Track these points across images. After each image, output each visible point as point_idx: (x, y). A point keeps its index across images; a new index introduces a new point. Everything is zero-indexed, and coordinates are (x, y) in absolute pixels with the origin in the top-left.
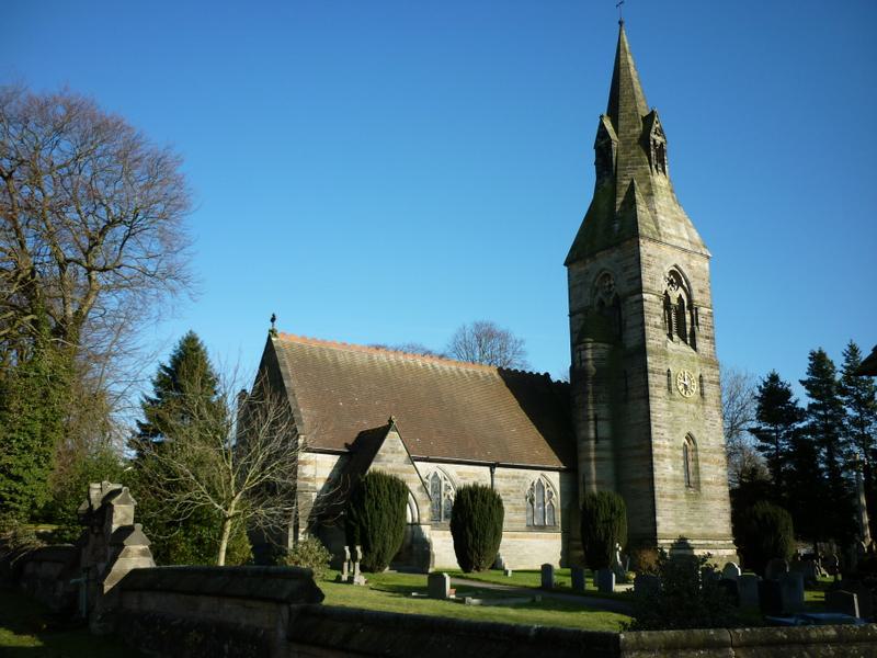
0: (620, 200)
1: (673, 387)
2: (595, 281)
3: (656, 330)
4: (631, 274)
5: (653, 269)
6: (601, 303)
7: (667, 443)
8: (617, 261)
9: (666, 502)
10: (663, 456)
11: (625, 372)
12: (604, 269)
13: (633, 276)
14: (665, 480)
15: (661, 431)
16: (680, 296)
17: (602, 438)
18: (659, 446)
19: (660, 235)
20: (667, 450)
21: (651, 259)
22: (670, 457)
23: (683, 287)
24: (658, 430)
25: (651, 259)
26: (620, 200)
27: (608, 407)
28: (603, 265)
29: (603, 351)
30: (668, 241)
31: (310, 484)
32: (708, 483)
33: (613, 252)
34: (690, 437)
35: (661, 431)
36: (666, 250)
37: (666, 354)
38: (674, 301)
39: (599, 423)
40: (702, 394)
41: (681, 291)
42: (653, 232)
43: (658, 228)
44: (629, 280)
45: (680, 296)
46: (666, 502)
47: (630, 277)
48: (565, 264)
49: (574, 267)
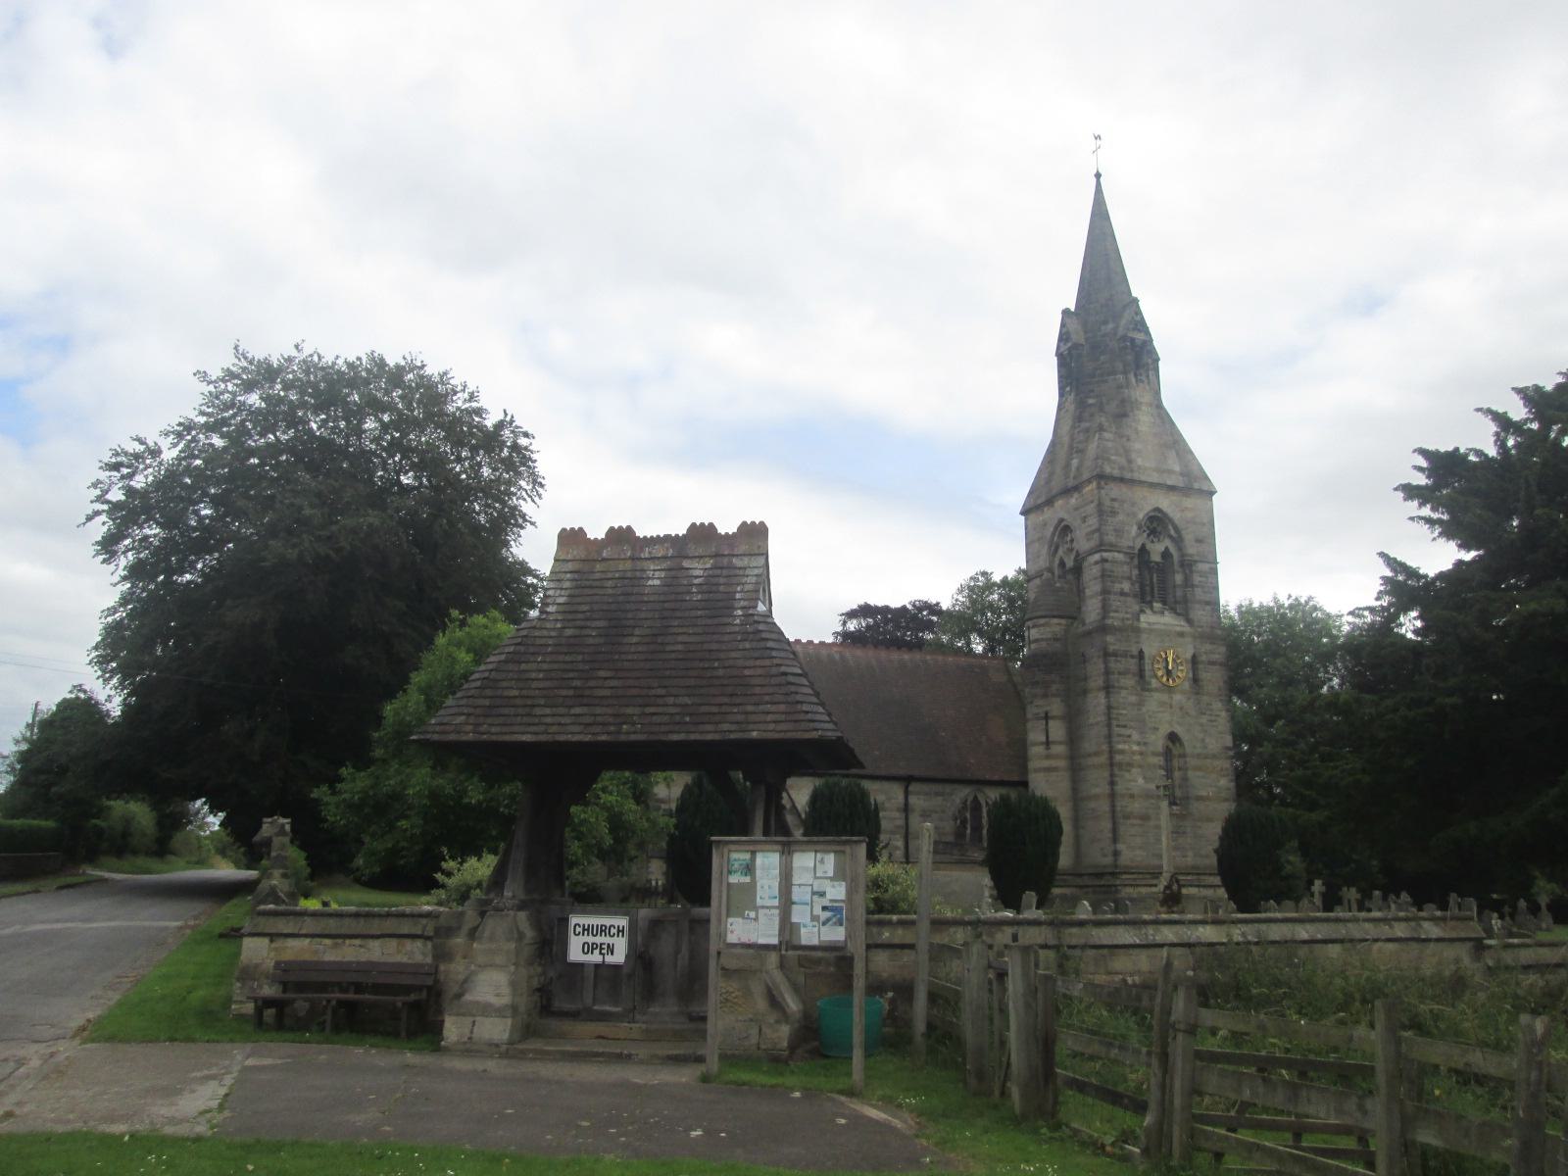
0: (289, 1060)
1: (1147, 673)
2: (1053, 534)
3: (1122, 598)
4: (1090, 526)
5: (1121, 517)
6: (1062, 564)
7: (1135, 748)
8: (1076, 509)
9: (1133, 825)
10: (1130, 765)
11: (1083, 655)
12: (1062, 520)
13: (1094, 528)
14: (1132, 796)
15: (1128, 732)
16: (1167, 548)
17: (1054, 743)
18: (1122, 752)
19: (1132, 471)
20: (1137, 757)
21: (1116, 505)
22: (1140, 766)
23: (1171, 537)
24: (1123, 731)
25: (1116, 505)
26: (289, 1060)
27: (1062, 701)
28: (1063, 514)
29: (1057, 629)
30: (1143, 478)
31: (1426, 511)
32: (1200, 798)
33: (1072, 496)
34: (1173, 737)
35: (1128, 732)
36: (1139, 493)
37: (1137, 631)
38: (1156, 558)
39: (1051, 723)
40: (1195, 680)
41: (1167, 543)
42: (1122, 468)
43: (1130, 461)
44: (1087, 534)
45: (1167, 548)
46: (1133, 825)
47: (1089, 529)
48: (1022, 513)
49: (1032, 516)
